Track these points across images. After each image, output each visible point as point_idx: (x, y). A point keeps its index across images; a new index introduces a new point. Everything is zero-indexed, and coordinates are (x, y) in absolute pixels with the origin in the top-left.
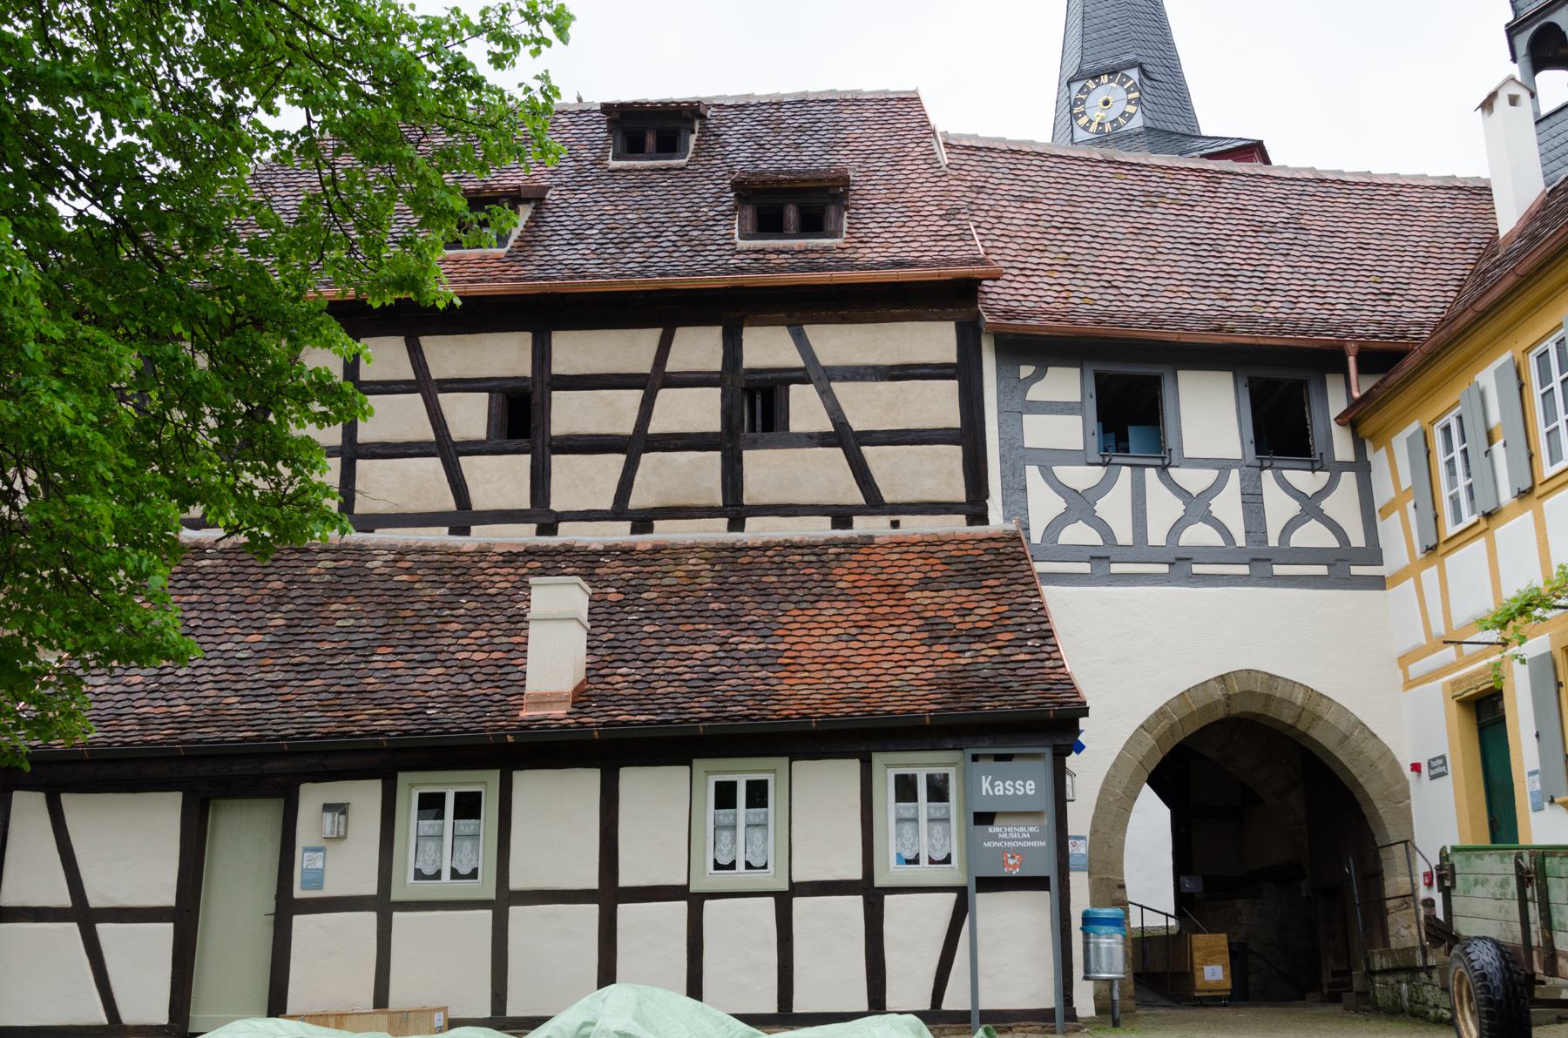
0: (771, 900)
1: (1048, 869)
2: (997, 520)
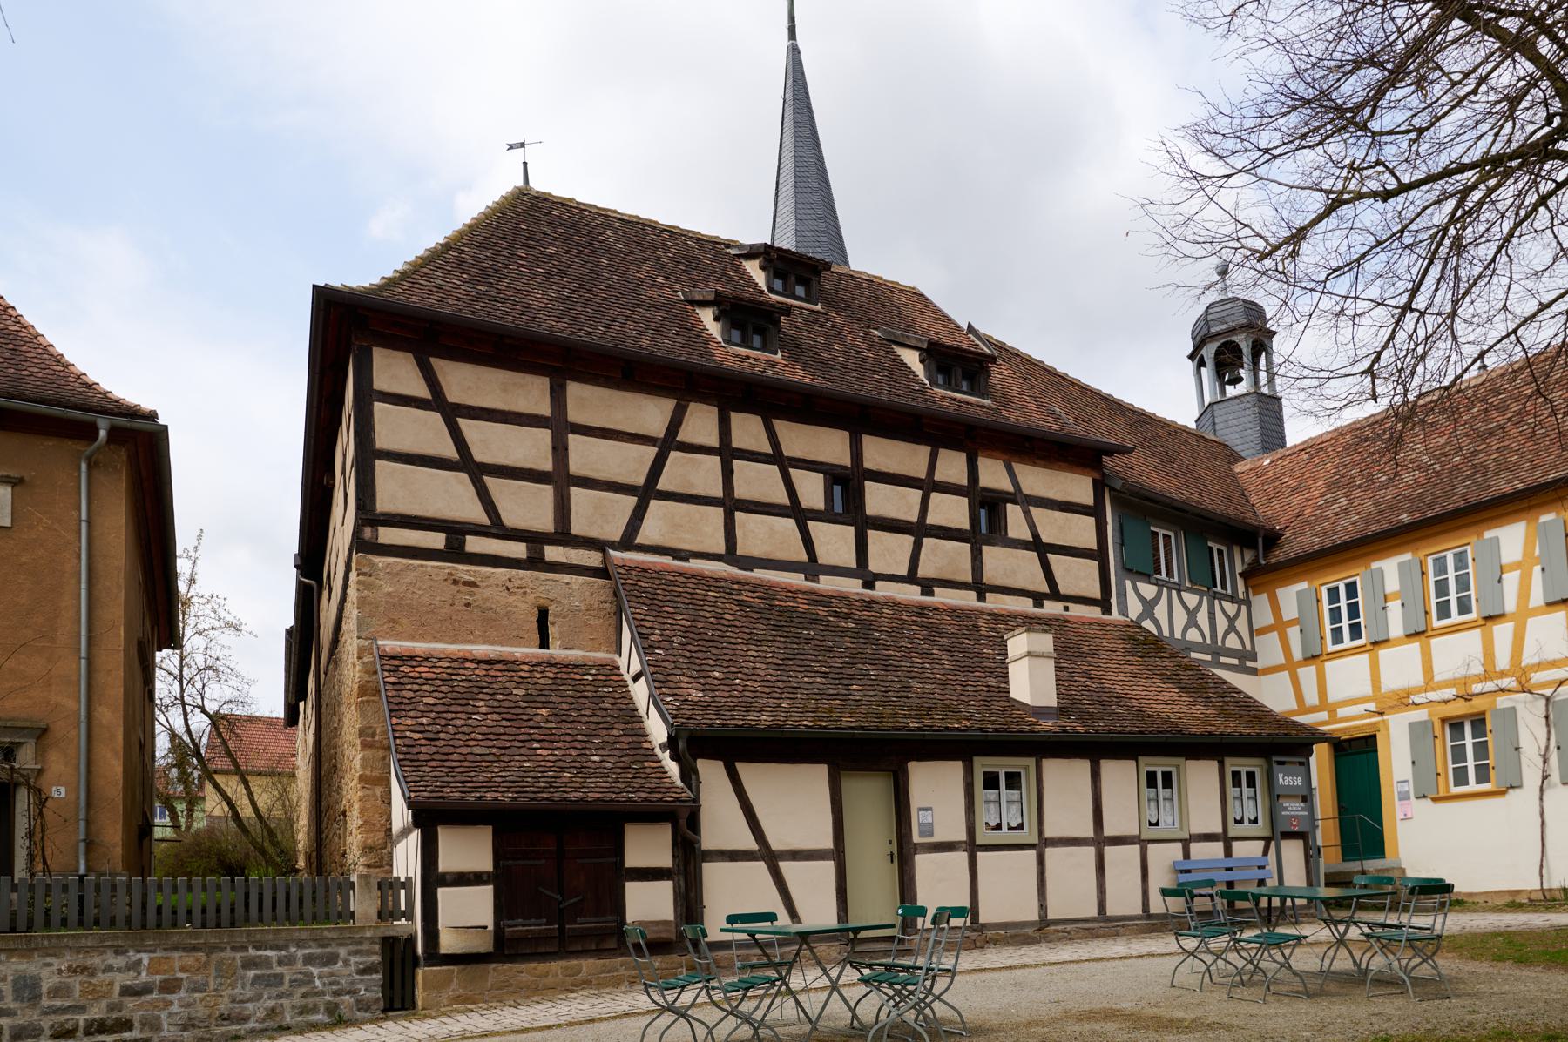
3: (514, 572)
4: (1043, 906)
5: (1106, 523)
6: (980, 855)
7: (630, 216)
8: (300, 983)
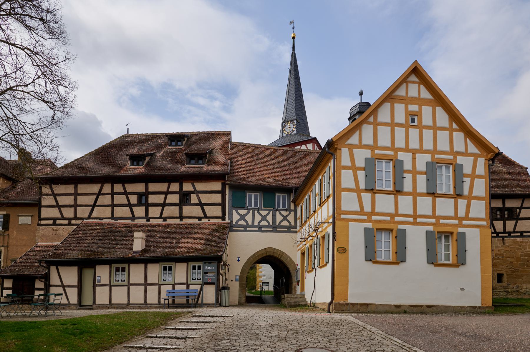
0: (171, 286)
1: (215, 281)
2: (227, 220)
3: (64, 227)
4: (129, 300)
5: (226, 195)
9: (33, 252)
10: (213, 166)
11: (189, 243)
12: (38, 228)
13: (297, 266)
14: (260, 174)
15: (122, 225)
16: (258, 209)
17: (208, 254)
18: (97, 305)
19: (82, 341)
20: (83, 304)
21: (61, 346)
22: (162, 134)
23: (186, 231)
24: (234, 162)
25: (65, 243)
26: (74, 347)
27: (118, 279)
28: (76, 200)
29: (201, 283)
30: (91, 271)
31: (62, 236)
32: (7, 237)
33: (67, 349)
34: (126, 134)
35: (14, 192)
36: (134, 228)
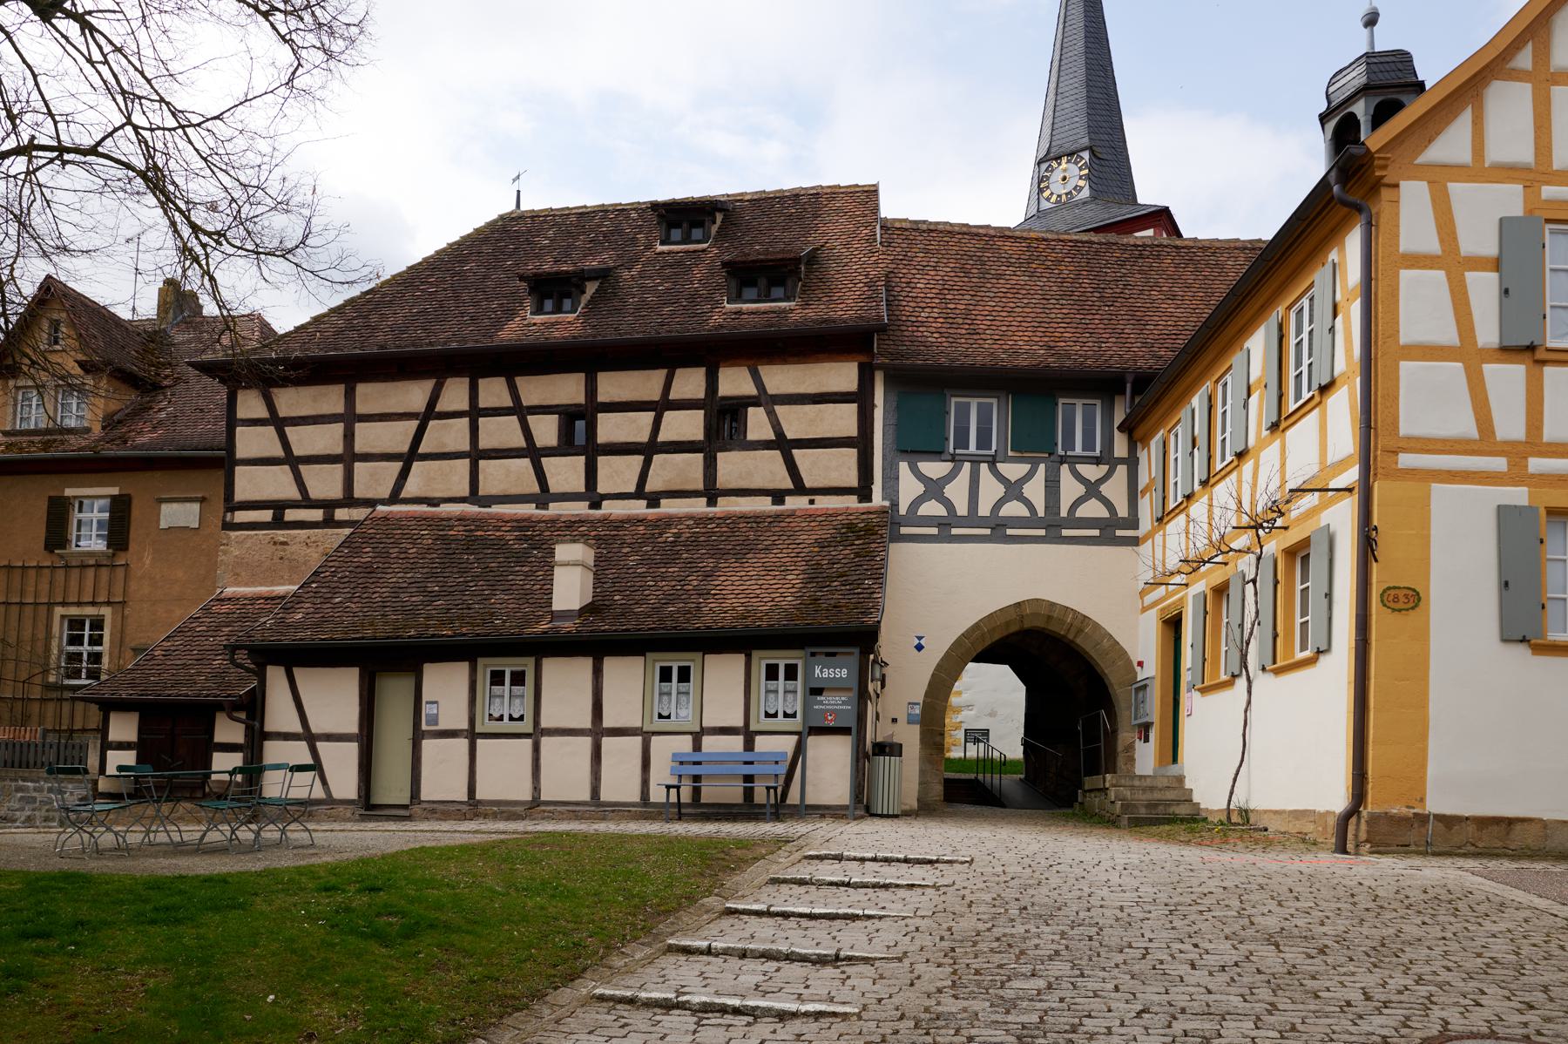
0: (689, 738)
2: (878, 499)
3: (312, 531)
4: (536, 788)
5: (873, 406)
6: (479, 741)
7: (870, 186)
8: (46, 803)
9: (208, 620)
10: (823, 307)
11: (748, 583)
12: (224, 536)
13: (1138, 669)
14: (994, 328)
15: (507, 522)
16: (990, 459)
17: (824, 621)
18: (424, 805)
19: (418, 968)
20: (376, 800)
21: (334, 994)
22: (637, 207)
23: (731, 539)
24: (898, 289)
25: (314, 585)
26: (389, 1001)
27: (501, 712)
28: (349, 437)
29: (800, 729)
30: (407, 684)
31: (305, 563)
32: (120, 572)
33: (360, 1009)
34: (512, 213)
35: (145, 422)
36: (549, 533)
